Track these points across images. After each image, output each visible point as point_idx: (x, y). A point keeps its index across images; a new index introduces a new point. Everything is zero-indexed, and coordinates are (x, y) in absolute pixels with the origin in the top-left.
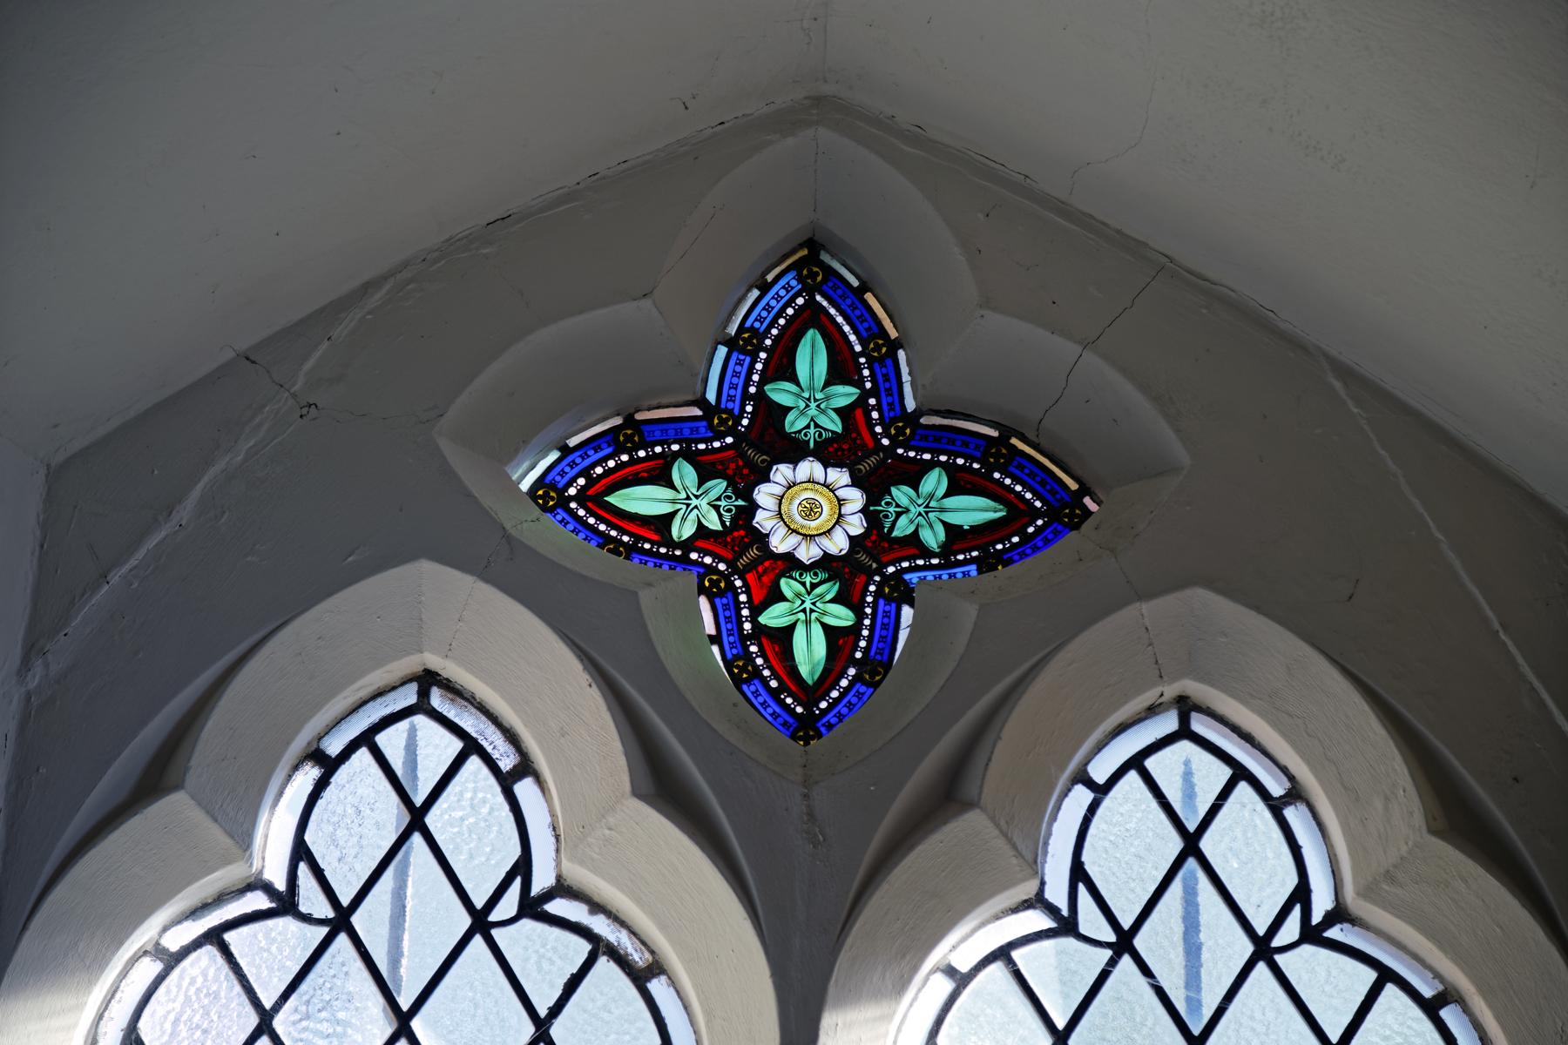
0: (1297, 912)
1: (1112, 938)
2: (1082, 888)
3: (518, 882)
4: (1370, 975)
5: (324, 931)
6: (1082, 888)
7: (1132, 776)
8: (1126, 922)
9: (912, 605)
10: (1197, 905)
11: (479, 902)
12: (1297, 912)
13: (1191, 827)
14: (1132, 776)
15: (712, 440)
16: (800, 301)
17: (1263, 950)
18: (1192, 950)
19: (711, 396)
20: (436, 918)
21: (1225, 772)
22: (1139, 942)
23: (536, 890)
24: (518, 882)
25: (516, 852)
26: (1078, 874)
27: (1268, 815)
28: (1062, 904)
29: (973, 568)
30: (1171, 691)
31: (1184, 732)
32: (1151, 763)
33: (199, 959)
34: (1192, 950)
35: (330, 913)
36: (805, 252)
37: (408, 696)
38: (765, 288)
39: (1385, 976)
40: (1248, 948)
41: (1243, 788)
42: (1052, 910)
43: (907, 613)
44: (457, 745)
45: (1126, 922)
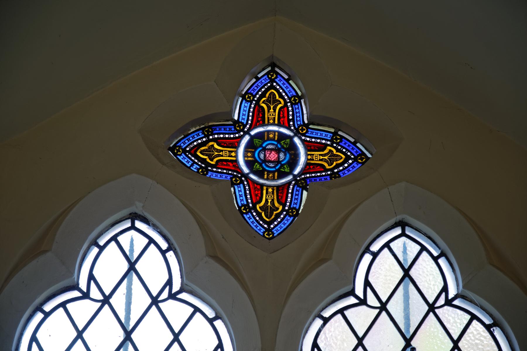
0: (443, 295)
1: (378, 305)
2: (368, 289)
3: (168, 288)
4: (468, 317)
5: (378, 311)
6: (368, 289)
7: (386, 250)
8: (384, 300)
9: (307, 191)
10: (127, 289)
11: (154, 294)
12: (443, 295)
13: (406, 267)
14: (386, 250)
15: (236, 134)
16: (269, 85)
17: (155, 301)
18: (129, 303)
19: (236, 118)
20: (141, 301)
21: (418, 248)
22: (388, 307)
23: (174, 291)
24: (168, 288)
25: (167, 277)
26: (367, 284)
27: (433, 262)
28: (85, 289)
29: (328, 178)
30: (399, 218)
31: (403, 234)
32: (392, 245)
33: (481, 328)
34: (129, 303)
35: (101, 298)
36: (269, 69)
37: (128, 224)
38: (258, 79)
39: (474, 317)
40: (149, 301)
41: (425, 253)
42: (357, 297)
43: (305, 193)
44: (146, 241)
45: (384, 300)
